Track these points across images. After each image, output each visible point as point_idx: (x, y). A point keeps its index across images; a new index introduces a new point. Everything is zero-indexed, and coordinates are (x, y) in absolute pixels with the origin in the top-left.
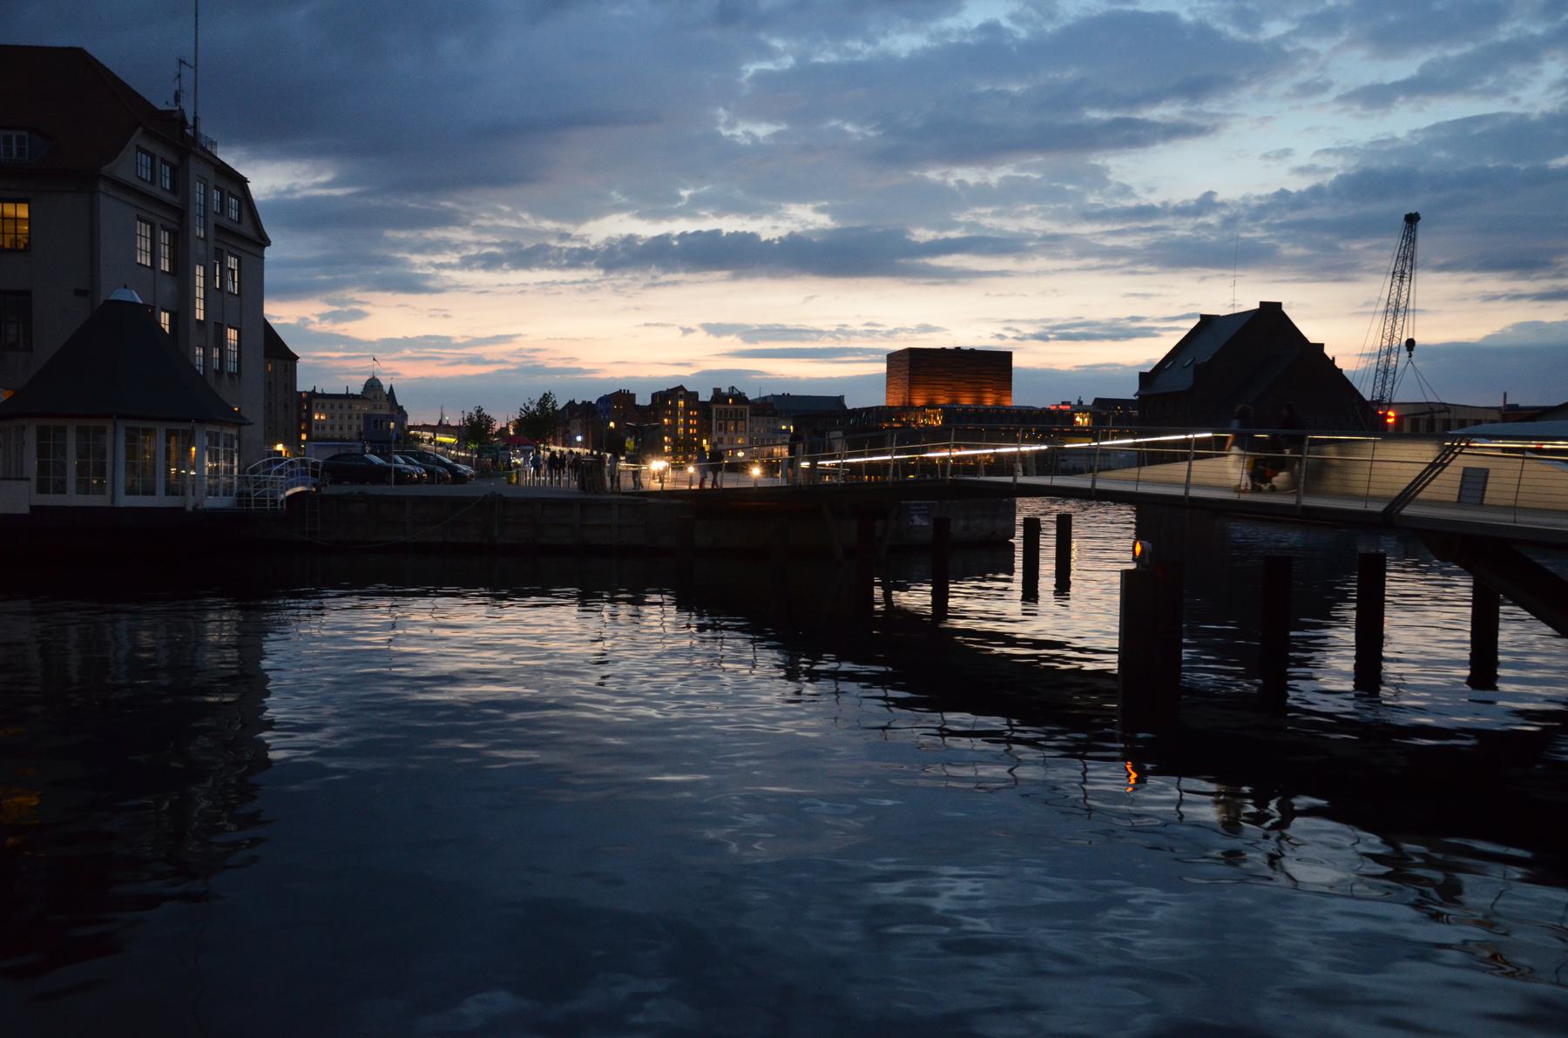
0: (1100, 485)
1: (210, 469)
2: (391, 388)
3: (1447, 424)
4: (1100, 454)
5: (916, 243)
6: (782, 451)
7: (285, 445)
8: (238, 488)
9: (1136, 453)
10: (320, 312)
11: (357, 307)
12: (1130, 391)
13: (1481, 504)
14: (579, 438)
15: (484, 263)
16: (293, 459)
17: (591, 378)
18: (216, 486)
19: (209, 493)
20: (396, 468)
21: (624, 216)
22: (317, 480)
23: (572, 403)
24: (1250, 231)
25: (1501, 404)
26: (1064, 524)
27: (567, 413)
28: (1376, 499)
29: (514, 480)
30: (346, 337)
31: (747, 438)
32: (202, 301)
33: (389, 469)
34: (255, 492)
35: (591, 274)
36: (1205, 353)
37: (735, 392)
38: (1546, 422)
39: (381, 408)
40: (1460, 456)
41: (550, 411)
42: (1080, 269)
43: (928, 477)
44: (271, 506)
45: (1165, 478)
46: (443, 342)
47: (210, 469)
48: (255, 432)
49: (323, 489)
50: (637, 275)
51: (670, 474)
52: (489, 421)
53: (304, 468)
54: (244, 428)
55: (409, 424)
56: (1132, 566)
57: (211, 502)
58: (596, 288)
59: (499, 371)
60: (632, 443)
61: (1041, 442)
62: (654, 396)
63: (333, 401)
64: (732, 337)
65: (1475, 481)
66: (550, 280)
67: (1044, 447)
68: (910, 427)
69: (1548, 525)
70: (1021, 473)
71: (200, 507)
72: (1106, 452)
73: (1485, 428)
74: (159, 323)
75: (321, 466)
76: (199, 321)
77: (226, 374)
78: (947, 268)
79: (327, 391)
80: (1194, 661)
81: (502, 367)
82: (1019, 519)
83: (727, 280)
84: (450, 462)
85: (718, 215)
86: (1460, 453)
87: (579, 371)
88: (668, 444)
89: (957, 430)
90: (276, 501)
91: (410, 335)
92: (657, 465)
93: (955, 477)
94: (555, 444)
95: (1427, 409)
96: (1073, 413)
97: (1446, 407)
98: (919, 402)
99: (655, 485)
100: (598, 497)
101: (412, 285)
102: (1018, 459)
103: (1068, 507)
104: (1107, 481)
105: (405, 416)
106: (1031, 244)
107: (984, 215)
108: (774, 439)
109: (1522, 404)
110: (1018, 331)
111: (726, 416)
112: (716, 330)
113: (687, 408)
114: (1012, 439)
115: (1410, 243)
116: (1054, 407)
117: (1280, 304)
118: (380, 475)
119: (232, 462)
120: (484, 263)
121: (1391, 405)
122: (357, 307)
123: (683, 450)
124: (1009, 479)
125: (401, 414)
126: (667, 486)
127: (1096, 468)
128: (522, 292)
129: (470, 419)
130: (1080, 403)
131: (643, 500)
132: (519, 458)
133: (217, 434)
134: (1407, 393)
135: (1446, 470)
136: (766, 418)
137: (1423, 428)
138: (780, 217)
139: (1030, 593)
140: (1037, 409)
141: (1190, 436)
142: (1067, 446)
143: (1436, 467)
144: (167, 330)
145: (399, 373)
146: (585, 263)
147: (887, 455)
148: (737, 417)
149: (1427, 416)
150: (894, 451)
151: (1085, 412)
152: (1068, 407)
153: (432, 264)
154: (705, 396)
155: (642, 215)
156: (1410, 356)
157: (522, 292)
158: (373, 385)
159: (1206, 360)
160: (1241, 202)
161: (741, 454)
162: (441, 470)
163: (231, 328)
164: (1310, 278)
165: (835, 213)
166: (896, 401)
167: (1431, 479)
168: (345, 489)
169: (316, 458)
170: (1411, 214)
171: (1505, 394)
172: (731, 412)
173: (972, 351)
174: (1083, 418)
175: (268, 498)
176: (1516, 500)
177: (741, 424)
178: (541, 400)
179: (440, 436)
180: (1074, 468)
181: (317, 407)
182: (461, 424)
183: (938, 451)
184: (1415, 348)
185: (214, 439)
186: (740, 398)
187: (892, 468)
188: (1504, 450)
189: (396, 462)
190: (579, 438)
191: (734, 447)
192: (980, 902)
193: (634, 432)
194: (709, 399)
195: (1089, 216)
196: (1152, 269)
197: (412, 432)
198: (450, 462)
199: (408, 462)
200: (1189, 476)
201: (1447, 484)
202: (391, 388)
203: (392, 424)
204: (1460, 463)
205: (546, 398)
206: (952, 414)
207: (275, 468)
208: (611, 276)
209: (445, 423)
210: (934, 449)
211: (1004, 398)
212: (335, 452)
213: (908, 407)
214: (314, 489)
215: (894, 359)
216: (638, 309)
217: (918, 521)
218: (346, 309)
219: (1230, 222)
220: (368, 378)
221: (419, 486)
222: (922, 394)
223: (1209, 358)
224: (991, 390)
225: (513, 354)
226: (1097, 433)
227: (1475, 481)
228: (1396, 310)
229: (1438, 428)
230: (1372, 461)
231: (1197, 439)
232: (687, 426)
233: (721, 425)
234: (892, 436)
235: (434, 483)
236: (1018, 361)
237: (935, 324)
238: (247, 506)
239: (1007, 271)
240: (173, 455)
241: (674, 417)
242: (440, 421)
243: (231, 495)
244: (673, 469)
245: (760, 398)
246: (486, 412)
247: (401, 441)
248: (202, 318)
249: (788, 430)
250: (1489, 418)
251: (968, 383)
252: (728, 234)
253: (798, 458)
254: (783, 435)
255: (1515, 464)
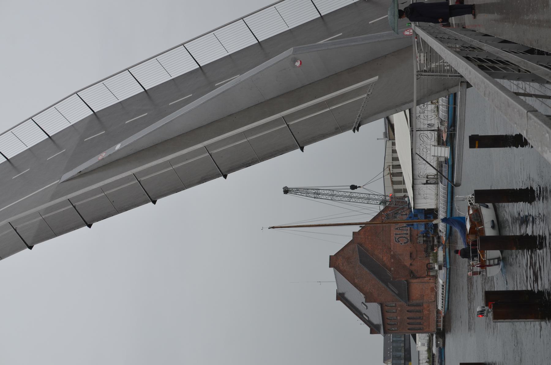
80: (513, 233)
115: (299, 191)
156: (360, 187)
170: (284, 191)
192: (435, 136)
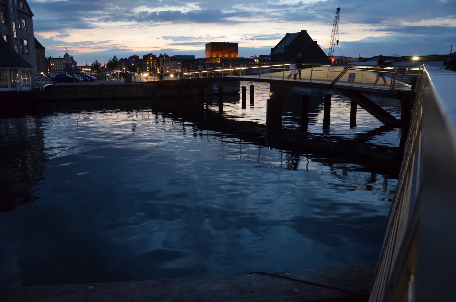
0: (261, 78)
1: (23, 80)
2: (72, 56)
3: (346, 62)
4: (261, 70)
5: (224, 14)
6: (179, 70)
7: (44, 72)
8: (32, 85)
9: (270, 69)
10: (56, 35)
11: (67, 33)
12: (268, 53)
13: (354, 82)
14: (124, 68)
15: (104, 20)
16: (46, 76)
17: (130, 52)
18: (25, 84)
19: (23, 86)
20: (75, 78)
21: (144, 7)
22: (53, 82)
23: (122, 59)
24: (311, 12)
25: (358, 57)
26: (252, 88)
27: (121, 62)
28: (329, 81)
29: (107, 80)
30: (64, 42)
31: (169, 67)
32: (15, 32)
33: (73, 78)
34: (36, 86)
35: (134, 23)
36: (288, 43)
37: (166, 55)
38: (373, 62)
39: (69, 62)
40: (349, 70)
41: (116, 61)
42: (266, 21)
43: (217, 76)
44: (41, 89)
45: (278, 76)
46: (91, 43)
47: (23, 80)
48: (35, 69)
49: (55, 84)
50: (147, 23)
51: (149, 77)
52: (99, 64)
53: (49, 79)
54: (31, 68)
55: (78, 66)
56: (269, 98)
57: (25, 89)
58: (134, 27)
59: (106, 50)
60: (139, 69)
61: (246, 67)
62: (144, 56)
63: (56, 60)
64: (170, 40)
65: (352, 76)
66: (122, 25)
67: (247, 68)
68: (212, 63)
69: (372, 87)
70: (241, 75)
71: (21, 90)
72: (263, 69)
73: (354, 63)
74: (3, 39)
75: (54, 78)
76: (15, 38)
77: (25, 53)
78: (231, 21)
79: (54, 57)
81: (107, 49)
82: (241, 86)
83: (171, 24)
84: (90, 76)
85: (169, 6)
86: (349, 69)
87: (128, 50)
88: (148, 69)
89: (224, 64)
90: (42, 88)
91: (82, 41)
92: (146, 75)
93: (224, 76)
94: (118, 70)
95: (341, 58)
96: (254, 59)
97: (346, 58)
98: (214, 56)
99: (145, 80)
100: (130, 84)
101: (84, 27)
102: (240, 71)
103: (254, 83)
104: (263, 77)
105: (76, 63)
106: (252, 14)
107: (240, 7)
108: (177, 67)
109: (363, 57)
110: (247, 37)
111: (163, 61)
112: (166, 38)
113: (153, 59)
114: (238, 66)
116: (249, 58)
117: (306, 31)
118: (70, 80)
119: (29, 78)
120: (104, 20)
121: (333, 57)
122: (67, 33)
123: (153, 71)
124: (238, 76)
125: (75, 63)
126: (149, 80)
127: (260, 73)
128: (115, 28)
129: (94, 64)
130: (256, 56)
131: (142, 84)
132: (108, 74)
133: (24, 70)
134: (337, 54)
135: (346, 73)
136: (174, 62)
137: (340, 63)
138: (186, 7)
139: (244, 107)
140: (245, 58)
141: (284, 65)
142: (253, 68)
143: (343, 73)
144: (6, 41)
145: (75, 52)
146: (133, 20)
147: (206, 71)
148: (167, 61)
149: (341, 60)
150: (208, 70)
151: (257, 59)
152: (253, 57)
153: (90, 20)
154: (158, 56)
155: (149, 6)
157: (115, 28)
158: (67, 55)
159: (288, 45)
160: (310, 4)
161: (168, 71)
162: (87, 78)
163: (25, 40)
164: (323, 24)
165: (200, 6)
166: (208, 56)
167: (342, 76)
168: (62, 84)
169: (53, 76)
171: (359, 55)
172: (165, 60)
173: (228, 43)
174: (257, 60)
175: (40, 87)
176: (361, 81)
177: (167, 63)
178: (113, 58)
179: (86, 69)
180: (254, 73)
181: (51, 62)
182: (92, 65)
183: (219, 70)
184: (339, 43)
185: (23, 71)
186: (167, 56)
187: (208, 74)
188: (359, 68)
189: (75, 76)
190: (124, 68)
191: (166, 69)
193: (139, 66)
194: (159, 57)
195: (271, 7)
196: (284, 21)
197: (79, 68)
198: (90, 76)
199: (78, 76)
200: (283, 75)
201: (346, 77)
202: (72, 56)
203: (73, 66)
204: (349, 72)
205: (115, 57)
206: (223, 60)
207: (41, 79)
208: (140, 23)
209: (87, 65)
210: (218, 69)
211: (236, 55)
212: (58, 74)
213: (211, 58)
214: (53, 84)
215: (208, 45)
216: (145, 33)
217: (215, 88)
218: (63, 34)
219: (306, 9)
220: (65, 53)
221: (81, 83)
222: (215, 54)
223: (289, 44)
224: (233, 53)
225: (110, 45)
226: (260, 64)
227: (352, 76)
228: (335, 32)
229: (344, 63)
230: (328, 71)
231: (285, 66)
232: (153, 64)
233: (162, 64)
234: (207, 66)
235: (85, 82)
236: (239, 46)
237: (225, 36)
238: (34, 90)
239: (246, 21)
240: (12, 76)
241: (149, 62)
242: (86, 65)
243: (30, 87)
244: (150, 76)
245: (172, 56)
246: (99, 62)
247: (76, 71)
248: (16, 37)
249: (180, 65)
250: (356, 61)
251: (226, 51)
252: (173, 11)
253: (183, 72)
254: (179, 66)
255: (361, 72)
